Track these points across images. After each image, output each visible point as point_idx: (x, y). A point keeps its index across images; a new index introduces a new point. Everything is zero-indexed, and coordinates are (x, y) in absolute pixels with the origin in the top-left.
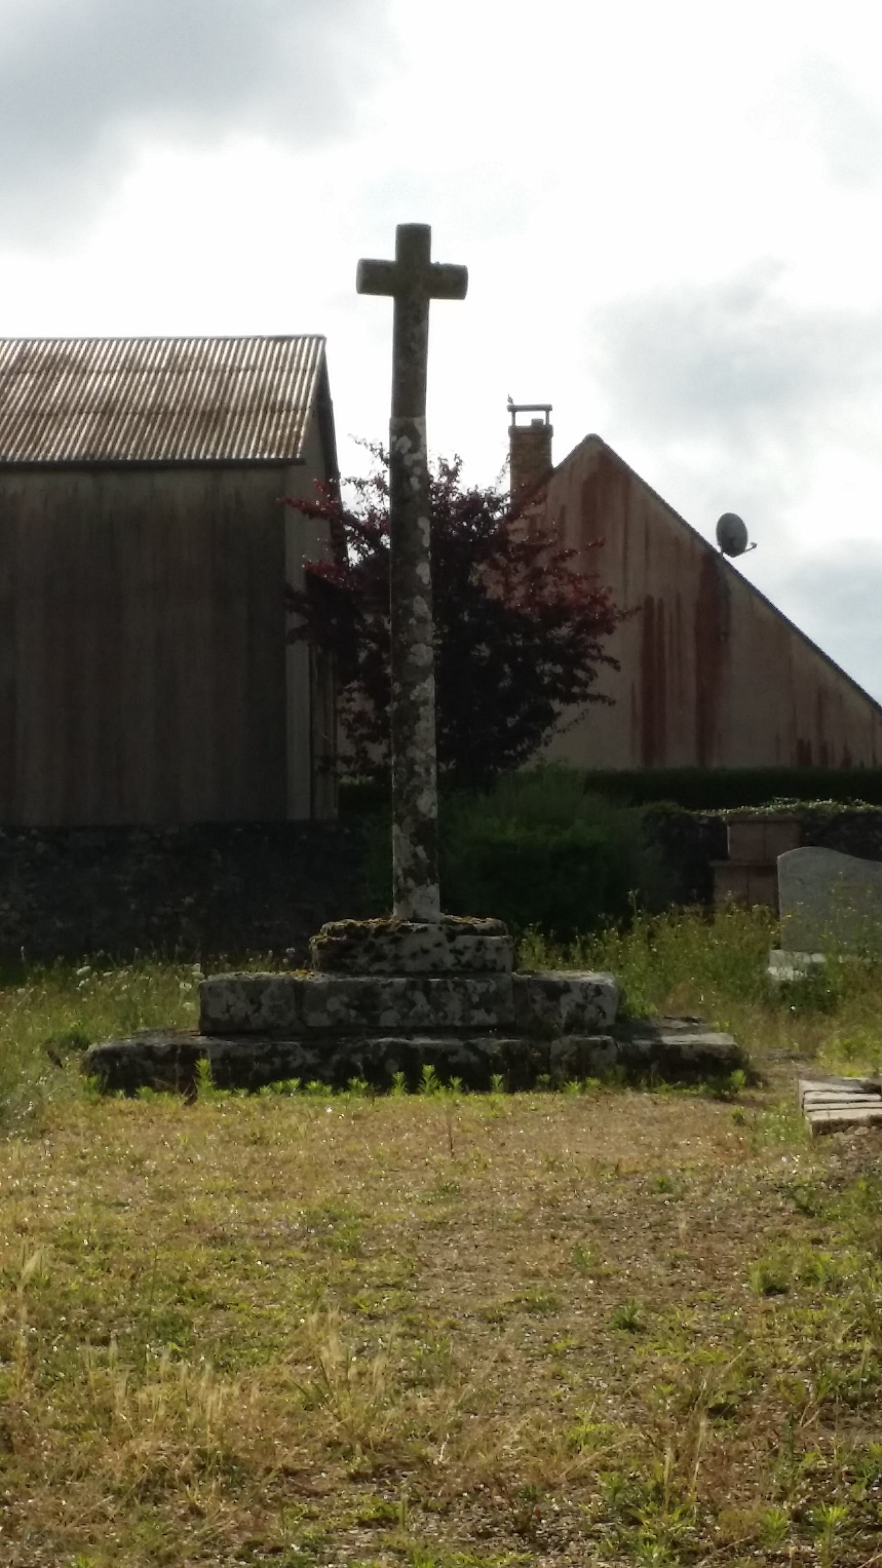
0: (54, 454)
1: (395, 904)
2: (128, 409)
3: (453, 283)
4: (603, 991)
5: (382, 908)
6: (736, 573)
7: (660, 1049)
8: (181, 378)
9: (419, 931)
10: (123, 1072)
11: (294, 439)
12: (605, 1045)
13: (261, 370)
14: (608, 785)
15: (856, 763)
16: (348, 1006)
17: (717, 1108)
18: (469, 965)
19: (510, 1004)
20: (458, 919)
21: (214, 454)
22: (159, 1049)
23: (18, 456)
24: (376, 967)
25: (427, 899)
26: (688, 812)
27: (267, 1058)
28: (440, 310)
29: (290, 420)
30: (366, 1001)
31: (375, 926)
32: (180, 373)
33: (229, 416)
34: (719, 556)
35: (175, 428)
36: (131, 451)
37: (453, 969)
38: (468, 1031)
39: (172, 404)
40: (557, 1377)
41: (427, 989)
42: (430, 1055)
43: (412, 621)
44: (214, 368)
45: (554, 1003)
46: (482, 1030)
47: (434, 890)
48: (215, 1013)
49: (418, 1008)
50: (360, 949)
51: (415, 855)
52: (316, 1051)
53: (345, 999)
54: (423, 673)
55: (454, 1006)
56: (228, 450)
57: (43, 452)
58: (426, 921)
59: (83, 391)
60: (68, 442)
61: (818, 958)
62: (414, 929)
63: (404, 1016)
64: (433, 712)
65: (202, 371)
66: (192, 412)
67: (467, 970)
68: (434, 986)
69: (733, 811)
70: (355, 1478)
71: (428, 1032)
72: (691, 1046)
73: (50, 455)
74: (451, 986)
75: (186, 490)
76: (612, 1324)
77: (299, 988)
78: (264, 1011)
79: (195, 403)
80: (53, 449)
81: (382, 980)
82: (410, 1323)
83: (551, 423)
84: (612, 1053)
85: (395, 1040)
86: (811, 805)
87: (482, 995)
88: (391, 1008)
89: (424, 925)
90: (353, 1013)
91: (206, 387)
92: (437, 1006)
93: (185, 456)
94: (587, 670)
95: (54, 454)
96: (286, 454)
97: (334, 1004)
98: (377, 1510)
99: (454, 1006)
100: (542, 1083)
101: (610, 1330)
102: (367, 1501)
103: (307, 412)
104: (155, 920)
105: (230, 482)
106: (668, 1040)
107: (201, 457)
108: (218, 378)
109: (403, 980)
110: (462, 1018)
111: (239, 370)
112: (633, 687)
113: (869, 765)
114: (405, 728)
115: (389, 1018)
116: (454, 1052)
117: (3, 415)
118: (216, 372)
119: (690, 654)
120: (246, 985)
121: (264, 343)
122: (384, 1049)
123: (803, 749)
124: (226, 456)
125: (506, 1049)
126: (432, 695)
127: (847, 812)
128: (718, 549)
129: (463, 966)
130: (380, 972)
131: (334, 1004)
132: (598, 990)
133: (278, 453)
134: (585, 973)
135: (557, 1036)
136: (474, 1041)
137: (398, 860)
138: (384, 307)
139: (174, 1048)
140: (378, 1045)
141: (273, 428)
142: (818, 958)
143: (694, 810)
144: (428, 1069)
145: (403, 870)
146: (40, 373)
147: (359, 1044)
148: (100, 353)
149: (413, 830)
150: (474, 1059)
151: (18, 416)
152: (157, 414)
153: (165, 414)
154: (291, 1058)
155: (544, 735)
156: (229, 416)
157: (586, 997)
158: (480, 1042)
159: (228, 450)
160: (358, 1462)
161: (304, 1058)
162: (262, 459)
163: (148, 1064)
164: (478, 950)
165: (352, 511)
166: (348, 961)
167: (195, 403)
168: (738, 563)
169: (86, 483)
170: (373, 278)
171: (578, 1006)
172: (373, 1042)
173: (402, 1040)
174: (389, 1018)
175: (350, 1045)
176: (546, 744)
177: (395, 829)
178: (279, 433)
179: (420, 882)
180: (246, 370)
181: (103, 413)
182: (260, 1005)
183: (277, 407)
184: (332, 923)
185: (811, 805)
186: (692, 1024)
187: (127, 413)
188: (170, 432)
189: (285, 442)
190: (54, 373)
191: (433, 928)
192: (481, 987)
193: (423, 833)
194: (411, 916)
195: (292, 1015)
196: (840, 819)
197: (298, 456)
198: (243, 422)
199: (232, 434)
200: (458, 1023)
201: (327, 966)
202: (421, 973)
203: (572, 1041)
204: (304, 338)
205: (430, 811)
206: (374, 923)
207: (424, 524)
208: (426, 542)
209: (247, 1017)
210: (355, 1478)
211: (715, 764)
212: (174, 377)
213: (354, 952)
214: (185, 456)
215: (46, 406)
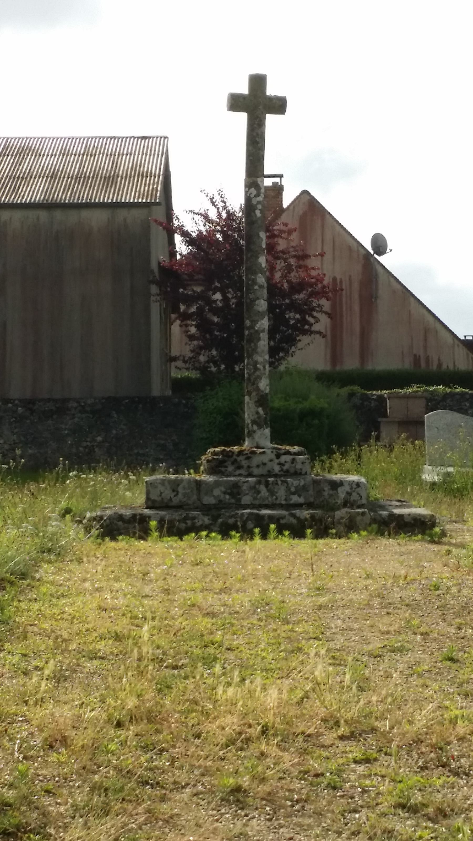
0: (26, 199)
1: (247, 439)
2: (64, 175)
3: (279, 106)
4: (361, 485)
5: (239, 441)
6: (382, 265)
7: (392, 515)
8: (92, 158)
9: (261, 453)
10: (114, 528)
11: (154, 192)
12: (363, 514)
13: (135, 155)
14: (322, 377)
15: (444, 367)
16: (225, 493)
17: (435, 548)
18: (287, 471)
19: (311, 492)
20: (280, 447)
21: (112, 199)
22: (126, 515)
23: (33, 200)
24: (238, 472)
25: (264, 436)
26: (366, 392)
27: (185, 520)
28: (271, 120)
29: (152, 182)
30: (235, 490)
31: (237, 450)
32: (91, 156)
33: (119, 179)
34: (372, 256)
35: (91, 186)
36: (68, 198)
37: (279, 473)
38: (289, 507)
39: (88, 173)
40: (425, 686)
41: (267, 484)
42: (272, 519)
43: (256, 287)
44: (109, 153)
45: (335, 491)
46: (299, 506)
47: (267, 431)
48: (154, 496)
49: (262, 494)
50: (229, 463)
51: (257, 413)
52: (210, 517)
53: (223, 489)
54: (261, 315)
55: (281, 492)
56: (119, 197)
57: (20, 199)
58: (263, 448)
59: (40, 165)
60: (33, 192)
61: (450, 469)
62: (258, 452)
63: (255, 499)
64: (267, 336)
65: (103, 155)
66: (99, 177)
67: (287, 473)
68: (270, 482)
69: (390, 391)
70: (342, 738)
71: (267, 507)
72: (409, 515)
73: (24, 199)
74: (280, 483)
75: (97, 219)
76: (440, 658)
77: (198, 484)
78: (180, 495)
79: (101, 172)
80: (25, 197)
81: (243, 479)
82: (333, 657)
83: (282, 184)
84: (367, 519)
85: (252, 511)
86: (431, 389)
87: (296, 487)
88: (247, 494)
89: (263, 450)
90: (227, 497)
91: (106, 165)
92: (272, 493)
93: (97, 201)
94: (314, 317)
95: (26, 199)
96: (151, 200)
97: (217, 492)
98: (362, 755)
99: (281, 492)
100: (333, 534)
101: (441, 661)
102: (355, 750)
103: (161, 177)
104: (81, 449)
105: (122, 214)
106: (397, 511)
107: (106, 201)
108: (112, 159)
109: (254, 479)
110: (286, 500)
111: (123, 155)
112: (326, 327)
113: (451, 367)
114: (252, 344)
115: (246, 500)
116: (283, 518)
117: (2, 178)
118: (111, 155)
119: (356, 308)
120: (170, 481)
121: (136, 140)
122: (246, 516)
123: (417, 360)
124: (119, 201)
125: (312, 516)
126: (267, 327)
127: (450, 392)
128: (372, 252)
129: (285, 472)
130: (240, 475)
131: (217, 492)
132: (358, 485)
133: (143, 199)
134: (348, 476)
135: (339, 509)
136: (294, 512)
137: (248, 415)
138: (242, 118)
139: (134, 516)
140: (243, 514)
141: (143, 185)
142: (450, 469)
143: (369, 391)
144: (273, 526)
145: (251, 420)
146: (16, 155)
147: (233, 513)
148: (39, 146)
149: (257, 399)
150: (294, 521)
151: (6, 178)
152: (80, 178)
153: (85, 177)
154: (196, 521)
155: (291, 352)
156: (119, 179)
157: (351, 489)
158: (297, 512)
159: (119, 197)
160: (343, 730)
161: (203, 520)
162: (142, 202)
163: (120, 523)
164: (292, 463)
165: (189, 230)
166: (223, 469)
167: (101, 172)
168: (381, 259)
169: (43, 215)
170: (236, 103)
171: (347, 493)
172: (240, 512)
173: (255, 511)
174: (246, 500)
175: (227, 514)
176: (292, 356)
177: (247, 398)
178: (146, 188)
179: (260, 427)
180: (127, 155)
181: (52, 177)
182: (178, 492)
183: (145, 174)
184: (214, 449)
185: (431, 389)
186: (402, 503)
187: (64, 178)
188: (88, 188)
189: (150, 193)
190: (24, 156)
191: (269, 452)
192: (296, 483)
193: (262, 401)
194: (255, 445)
195: (195, 497)
196: (446, 396)
197: (157, 201)
198: (127, 183)
199: (121, 189)
200: (284, 502)
201: (212, 471)
202: (262, 476)
203: (347, 512)
204: (123, 138)
205: (265, 389)
206: (236, 449)
207: (263, 235)
208: (264, 246)
209: (171, 499)
210: (342, 738)
211: (369, 367)
212: (88, 158)
213: (226, 464)
214: (97, 201)
215: (21, 173)
